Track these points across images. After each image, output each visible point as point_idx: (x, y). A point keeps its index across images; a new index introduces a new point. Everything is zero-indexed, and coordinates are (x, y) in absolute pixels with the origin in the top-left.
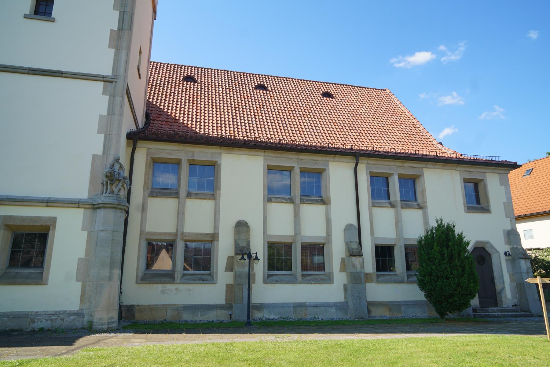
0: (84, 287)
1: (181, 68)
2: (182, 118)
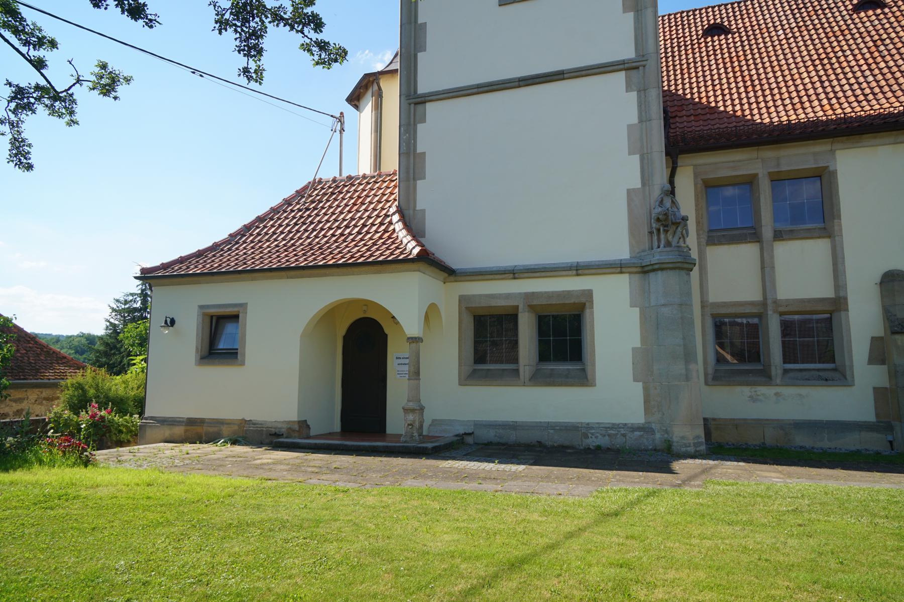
0: (646, 390)
1: (695, 15)
2: (721, 104)
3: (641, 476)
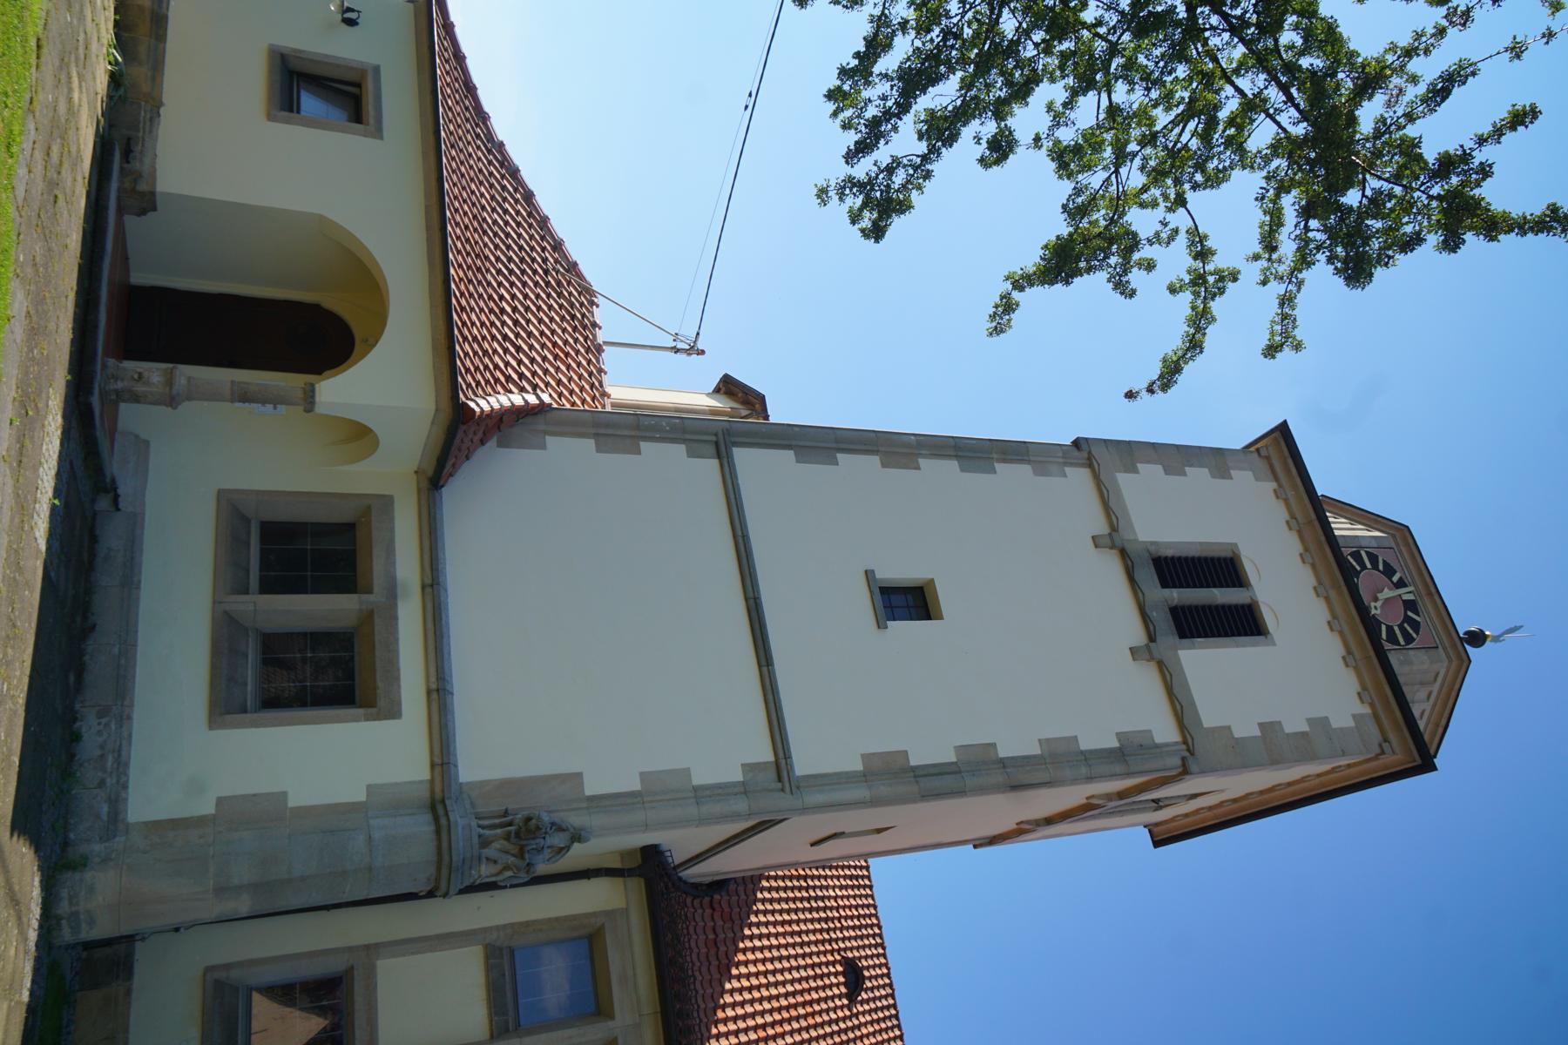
0: (201, 821)
1: (876, 946)
3: (20, 679)
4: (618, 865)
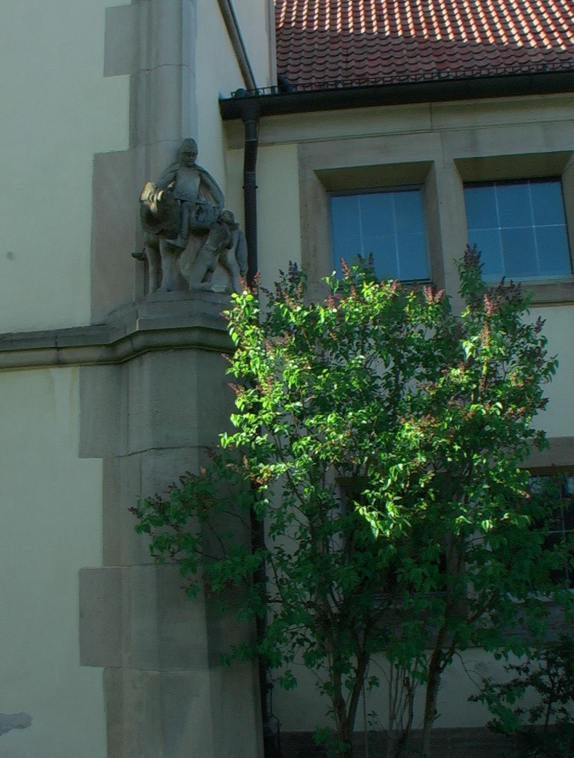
4: (241, 153)
